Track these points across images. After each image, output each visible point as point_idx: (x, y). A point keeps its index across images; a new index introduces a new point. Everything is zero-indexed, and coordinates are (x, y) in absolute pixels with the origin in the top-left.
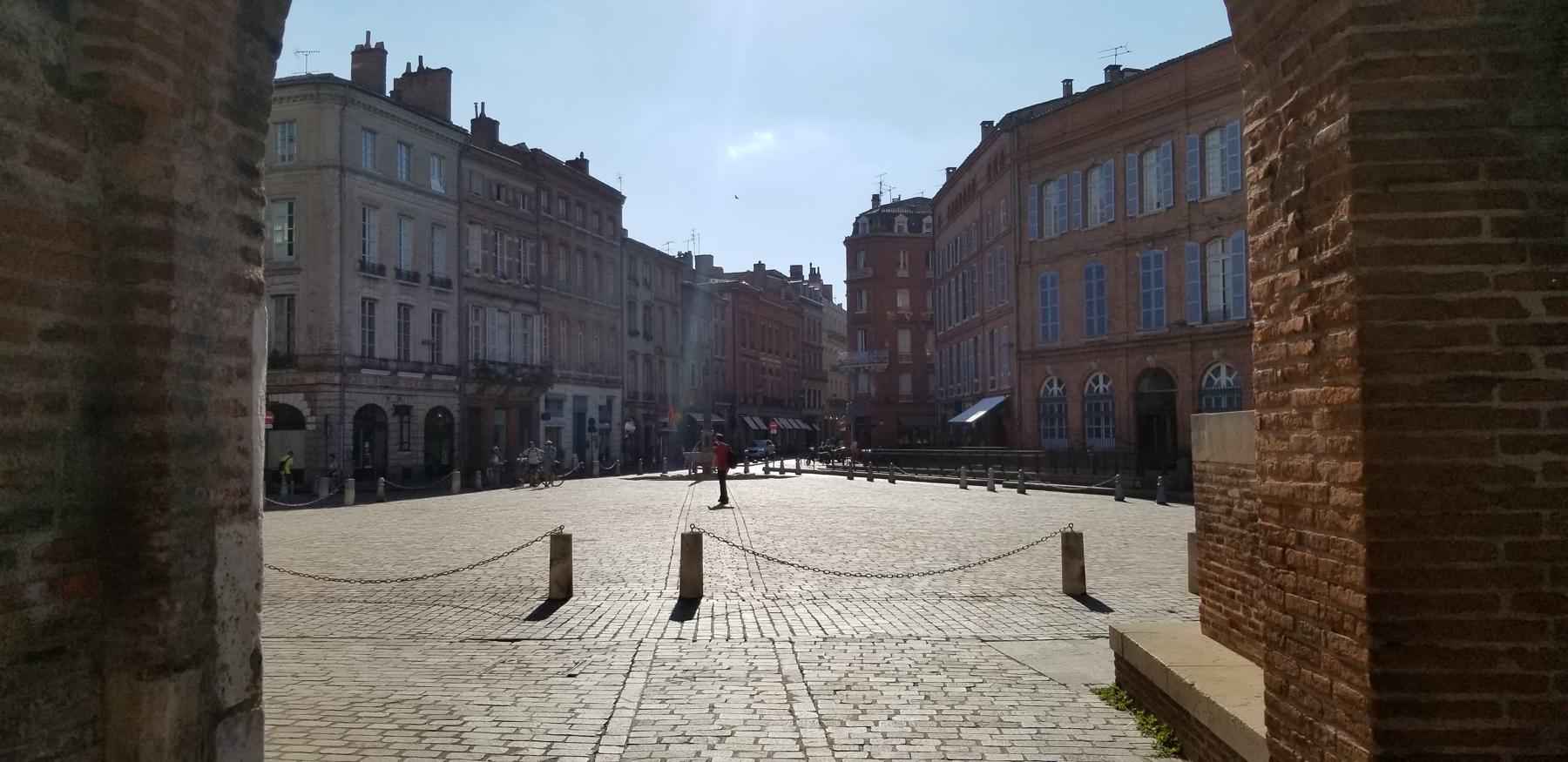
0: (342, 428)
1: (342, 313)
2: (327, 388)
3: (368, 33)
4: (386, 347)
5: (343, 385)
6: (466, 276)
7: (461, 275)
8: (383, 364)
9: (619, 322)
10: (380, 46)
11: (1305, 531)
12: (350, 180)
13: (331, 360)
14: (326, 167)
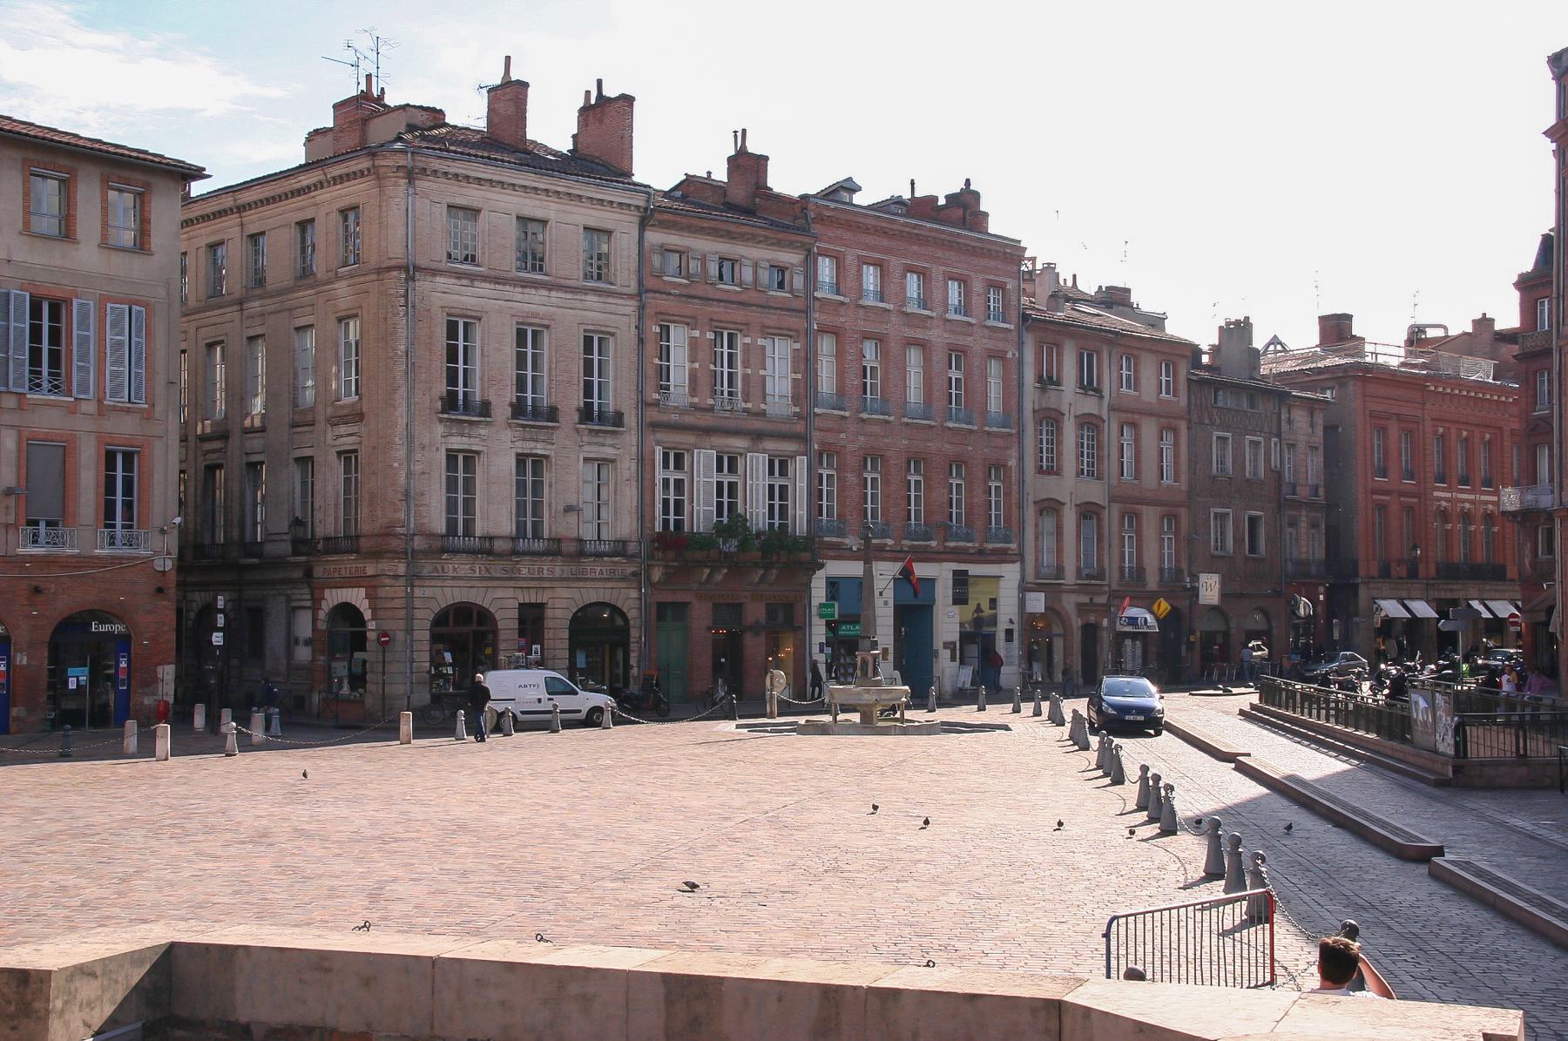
1: (409, 474)
2: (387, 581)
5: (412, 578)
6: (652, 405)
8: (486, 549)
9: (1014, 453)
11: (225, 1037)
12: (423, 284)
14: (389, 269)
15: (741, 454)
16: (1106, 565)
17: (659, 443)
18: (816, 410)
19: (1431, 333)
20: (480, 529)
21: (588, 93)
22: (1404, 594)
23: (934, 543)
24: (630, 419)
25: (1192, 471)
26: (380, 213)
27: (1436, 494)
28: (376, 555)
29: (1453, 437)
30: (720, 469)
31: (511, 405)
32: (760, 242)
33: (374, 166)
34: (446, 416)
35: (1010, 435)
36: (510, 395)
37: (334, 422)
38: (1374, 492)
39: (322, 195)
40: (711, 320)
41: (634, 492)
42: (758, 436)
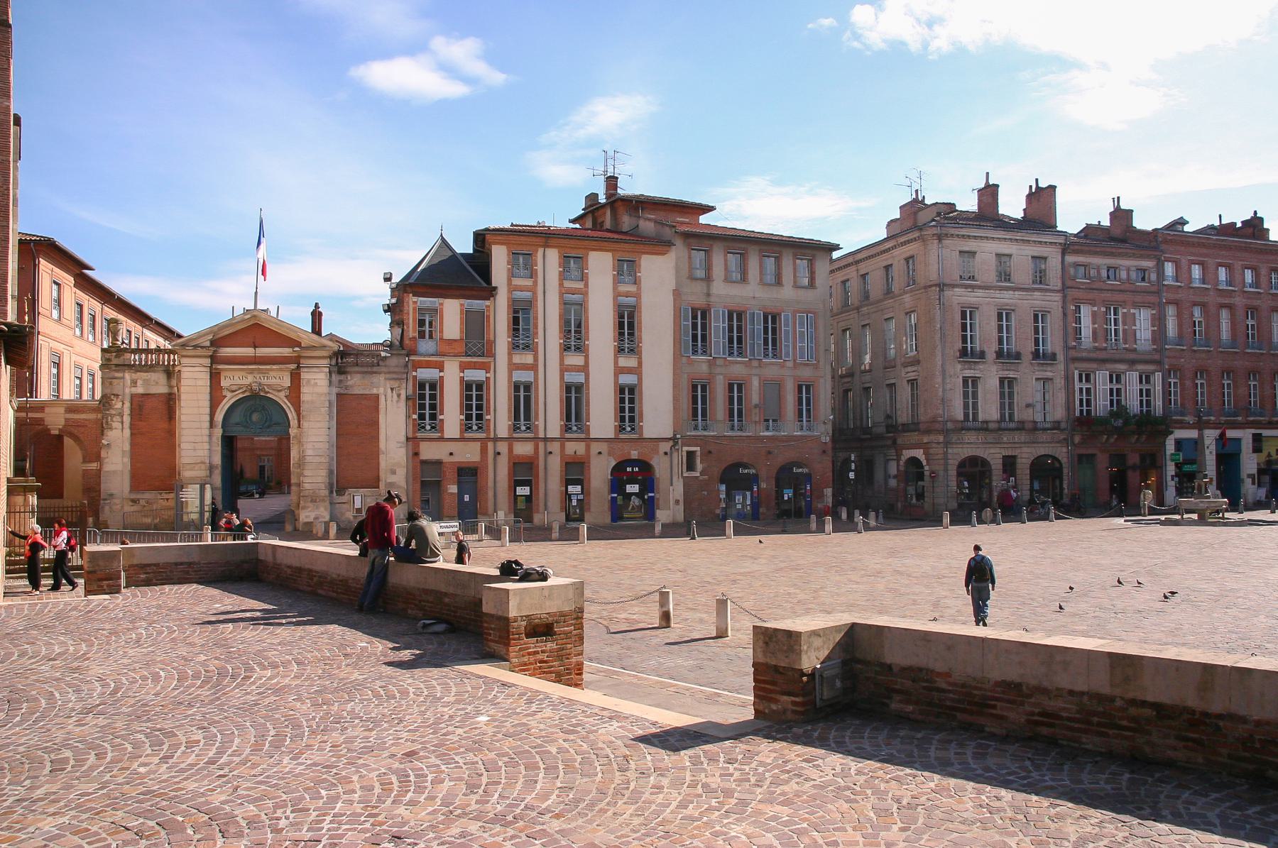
1: (944, 390)
4: (989, 410)
5: (947, 444)
7: (1067, 348)
12: (948, 293)
13: (937, 426)
14: (930, 286)
17: (1076, 369)
21: (1031, 187)
24: (1060, 357)
30: (1111, 381)
36: (995, 347)
37: (905, 365)
39: (896, 252)
42: (1132, 363)
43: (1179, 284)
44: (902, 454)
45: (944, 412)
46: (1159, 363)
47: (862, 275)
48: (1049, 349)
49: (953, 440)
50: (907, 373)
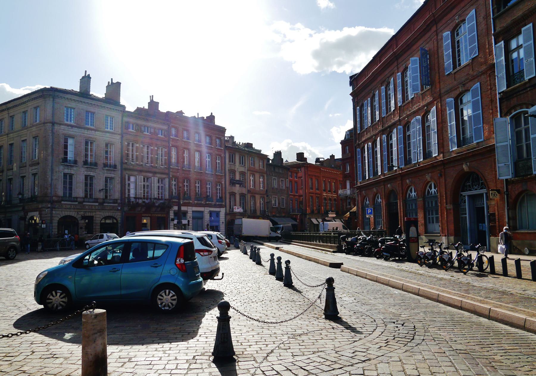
0: (51, 225)
1: (52, 180)
3: (86, 71)
5: (52, 208)
9: (223, 180)
10: (89, 75)
12: (56, 127)
14: (47, 123)
15: (150, 177)
16: (247, 209)
17: (127, 174)
18: (171, 167)
19: (321, 160)
20: (74, 195)
21: (109, 82)
22: (317, 217)
23: (203, 202)
24: (119, 167)
25: (267, 187)
26: (304, 334)
27: (323, 194)
28: (42, 202)
29: (327, 181)
30: (144, 181)
31: (83, 161)
32: (156, 122)
33: (43, 95)
34: (63, 164)
35: (222, 175)
36: (83, 159)
37: (31, 165)
38: (310, 193)
39: (30, 104)
40: (142, 142)
41: (120, 187)
42: (155, 173)
43: (178, 138)
44: (27, 215)
45: (51, 191)
46: (168, 174)
47: (11, 117)
48: (112, 162)
49: (56, 207)
50: (33, 170)
